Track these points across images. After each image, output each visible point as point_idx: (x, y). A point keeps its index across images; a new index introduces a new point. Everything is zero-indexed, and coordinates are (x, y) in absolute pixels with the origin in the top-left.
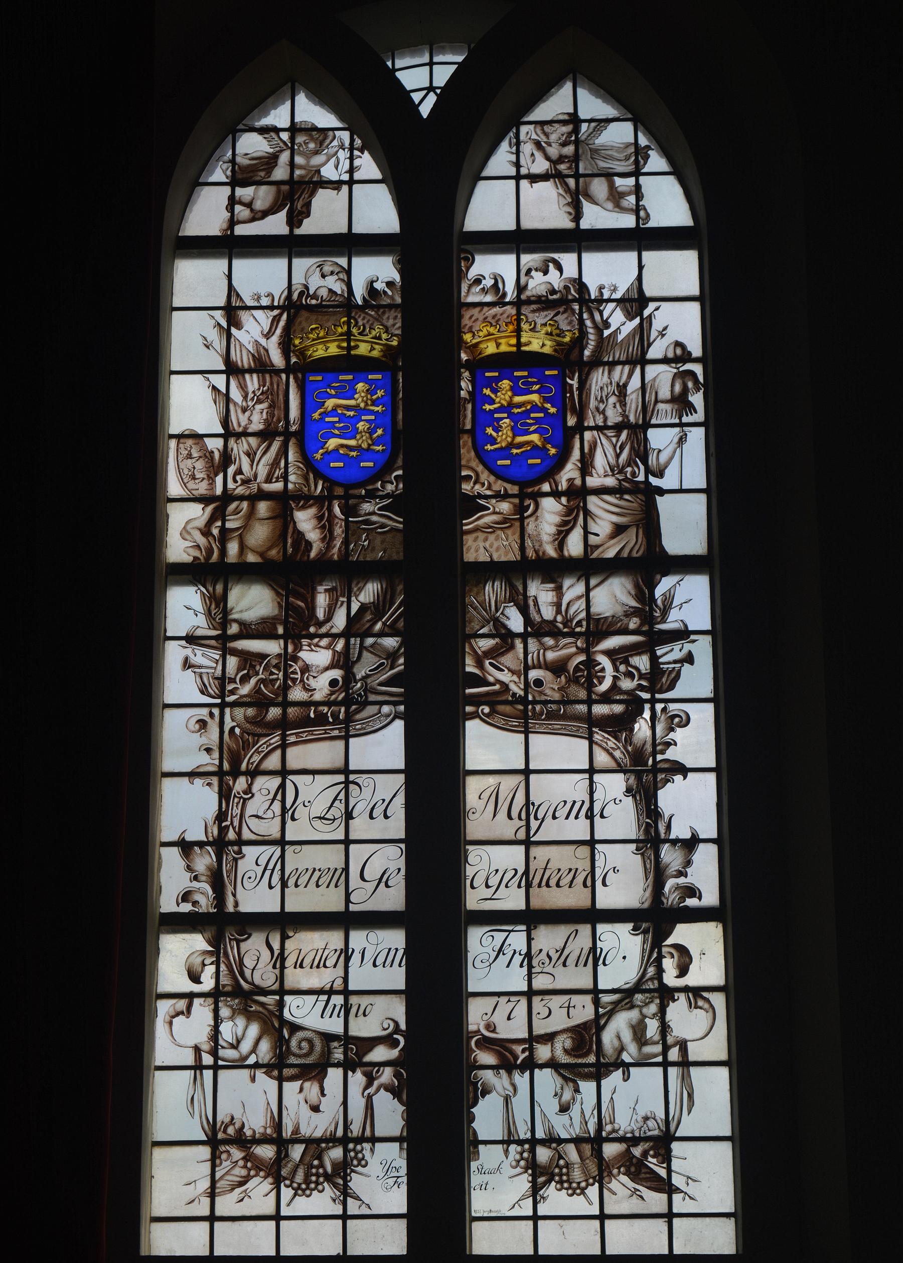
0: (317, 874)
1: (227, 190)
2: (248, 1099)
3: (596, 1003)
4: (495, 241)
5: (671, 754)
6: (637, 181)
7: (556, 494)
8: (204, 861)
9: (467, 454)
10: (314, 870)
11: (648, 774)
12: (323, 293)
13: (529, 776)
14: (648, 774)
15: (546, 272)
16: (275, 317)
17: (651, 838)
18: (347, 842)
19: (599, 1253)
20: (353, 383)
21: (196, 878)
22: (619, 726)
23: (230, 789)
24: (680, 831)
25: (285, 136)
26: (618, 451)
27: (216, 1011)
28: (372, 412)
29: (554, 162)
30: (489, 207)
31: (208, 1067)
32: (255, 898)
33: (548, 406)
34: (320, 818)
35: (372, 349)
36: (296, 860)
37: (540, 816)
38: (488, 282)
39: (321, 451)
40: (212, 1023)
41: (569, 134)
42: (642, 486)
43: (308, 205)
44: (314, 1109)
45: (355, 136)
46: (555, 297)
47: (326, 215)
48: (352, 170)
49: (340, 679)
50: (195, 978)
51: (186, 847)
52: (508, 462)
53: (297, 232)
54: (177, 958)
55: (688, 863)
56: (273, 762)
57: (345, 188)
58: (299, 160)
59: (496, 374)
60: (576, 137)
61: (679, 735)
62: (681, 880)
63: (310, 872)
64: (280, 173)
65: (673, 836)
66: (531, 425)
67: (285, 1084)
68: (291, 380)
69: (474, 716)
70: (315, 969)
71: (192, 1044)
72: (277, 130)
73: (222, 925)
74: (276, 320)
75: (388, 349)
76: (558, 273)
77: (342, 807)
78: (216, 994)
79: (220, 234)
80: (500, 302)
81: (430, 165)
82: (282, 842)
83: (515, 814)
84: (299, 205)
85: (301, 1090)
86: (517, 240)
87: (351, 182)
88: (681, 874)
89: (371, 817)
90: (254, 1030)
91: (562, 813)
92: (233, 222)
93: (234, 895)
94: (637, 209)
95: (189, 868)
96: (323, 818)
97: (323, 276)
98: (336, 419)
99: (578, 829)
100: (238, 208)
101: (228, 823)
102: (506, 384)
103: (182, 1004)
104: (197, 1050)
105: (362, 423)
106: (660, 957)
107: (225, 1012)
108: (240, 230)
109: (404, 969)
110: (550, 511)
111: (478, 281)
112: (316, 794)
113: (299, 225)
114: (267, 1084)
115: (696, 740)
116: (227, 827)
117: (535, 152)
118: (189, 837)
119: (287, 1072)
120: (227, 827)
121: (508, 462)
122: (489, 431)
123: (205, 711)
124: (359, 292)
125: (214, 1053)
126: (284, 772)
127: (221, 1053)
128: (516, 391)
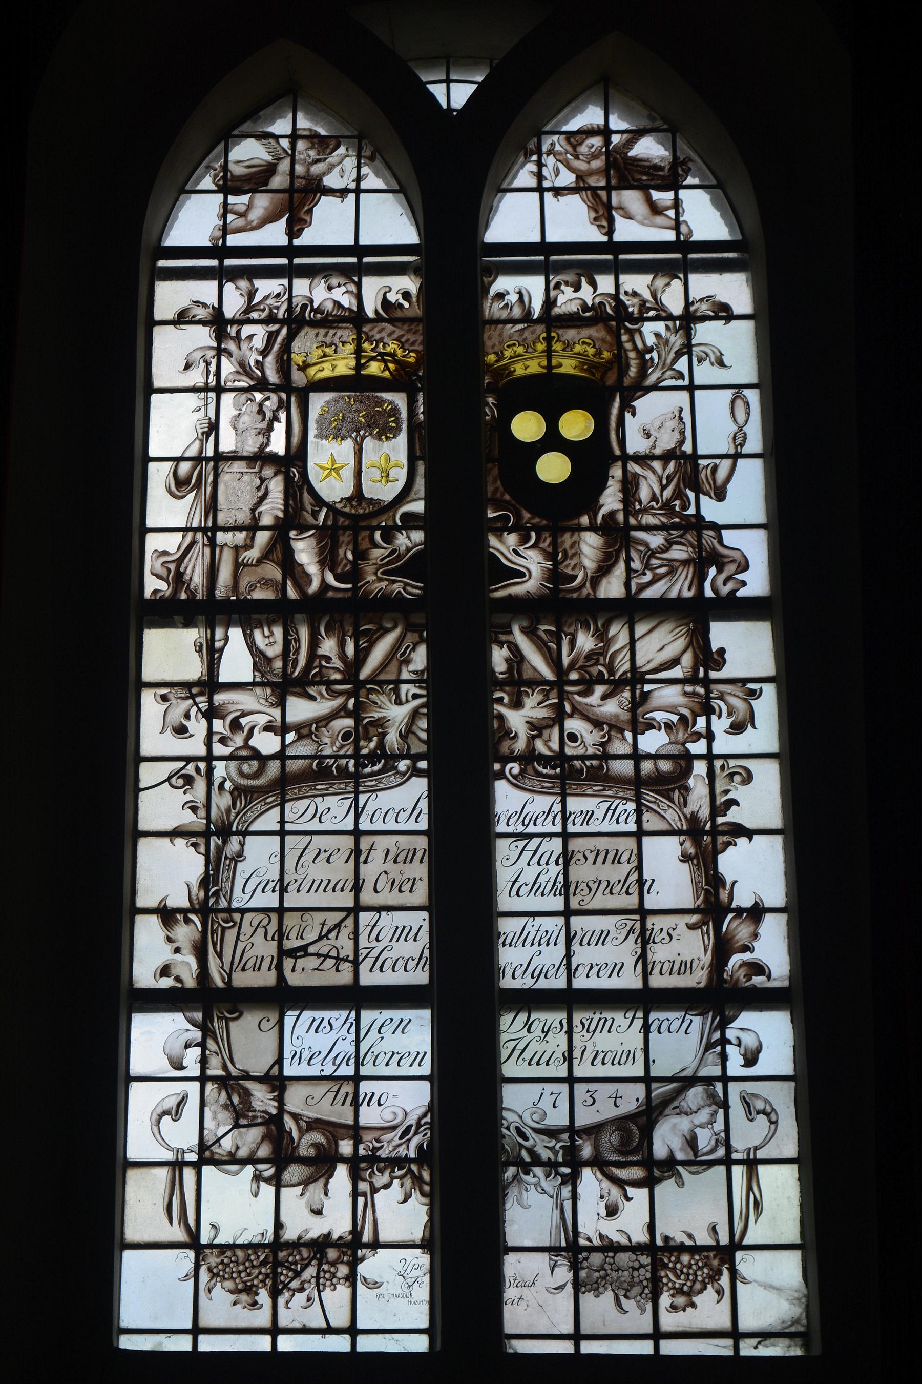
5: (733, 815)
6: (676, 195)
7: (593, 528)
8: (185, 933)
11: (706, 841)
12: (329, 306)
14: (706, 841)
15: (577, 288)
17: (713, 905)
19: (652, 1353)
21: (177, 950)
22: (672, 783)
24: (743, 899)
25: (285, 143)
26: (664, 482)
30: (512, 220)
42: (693, 520)
45: (684, 183)
46: (588, 314)
47: (329, 224)
48: (359, 179)
51: (167, 915)
53: (296, 242)
54: (154, 1040)
57: (352, 197)
58: (299, 169)
62: (747, 956)
64: (278, 181)
68: (293, 399)
70: (338, 892)
72: (277, 137)
73: (209, 1002)
74: (271, 337)
76: (591, 289)
79: (210, 244)
81: (450, 180)
86: (542, 256)
87: (358, 191)
88: (746, 949)
92: (225, 230)
94: (677, 226)
97: (330, 288)
100: (230, 217)
108: (233, 240)
110: (590, 545)
115: (761, 799)
118: (171, 903)
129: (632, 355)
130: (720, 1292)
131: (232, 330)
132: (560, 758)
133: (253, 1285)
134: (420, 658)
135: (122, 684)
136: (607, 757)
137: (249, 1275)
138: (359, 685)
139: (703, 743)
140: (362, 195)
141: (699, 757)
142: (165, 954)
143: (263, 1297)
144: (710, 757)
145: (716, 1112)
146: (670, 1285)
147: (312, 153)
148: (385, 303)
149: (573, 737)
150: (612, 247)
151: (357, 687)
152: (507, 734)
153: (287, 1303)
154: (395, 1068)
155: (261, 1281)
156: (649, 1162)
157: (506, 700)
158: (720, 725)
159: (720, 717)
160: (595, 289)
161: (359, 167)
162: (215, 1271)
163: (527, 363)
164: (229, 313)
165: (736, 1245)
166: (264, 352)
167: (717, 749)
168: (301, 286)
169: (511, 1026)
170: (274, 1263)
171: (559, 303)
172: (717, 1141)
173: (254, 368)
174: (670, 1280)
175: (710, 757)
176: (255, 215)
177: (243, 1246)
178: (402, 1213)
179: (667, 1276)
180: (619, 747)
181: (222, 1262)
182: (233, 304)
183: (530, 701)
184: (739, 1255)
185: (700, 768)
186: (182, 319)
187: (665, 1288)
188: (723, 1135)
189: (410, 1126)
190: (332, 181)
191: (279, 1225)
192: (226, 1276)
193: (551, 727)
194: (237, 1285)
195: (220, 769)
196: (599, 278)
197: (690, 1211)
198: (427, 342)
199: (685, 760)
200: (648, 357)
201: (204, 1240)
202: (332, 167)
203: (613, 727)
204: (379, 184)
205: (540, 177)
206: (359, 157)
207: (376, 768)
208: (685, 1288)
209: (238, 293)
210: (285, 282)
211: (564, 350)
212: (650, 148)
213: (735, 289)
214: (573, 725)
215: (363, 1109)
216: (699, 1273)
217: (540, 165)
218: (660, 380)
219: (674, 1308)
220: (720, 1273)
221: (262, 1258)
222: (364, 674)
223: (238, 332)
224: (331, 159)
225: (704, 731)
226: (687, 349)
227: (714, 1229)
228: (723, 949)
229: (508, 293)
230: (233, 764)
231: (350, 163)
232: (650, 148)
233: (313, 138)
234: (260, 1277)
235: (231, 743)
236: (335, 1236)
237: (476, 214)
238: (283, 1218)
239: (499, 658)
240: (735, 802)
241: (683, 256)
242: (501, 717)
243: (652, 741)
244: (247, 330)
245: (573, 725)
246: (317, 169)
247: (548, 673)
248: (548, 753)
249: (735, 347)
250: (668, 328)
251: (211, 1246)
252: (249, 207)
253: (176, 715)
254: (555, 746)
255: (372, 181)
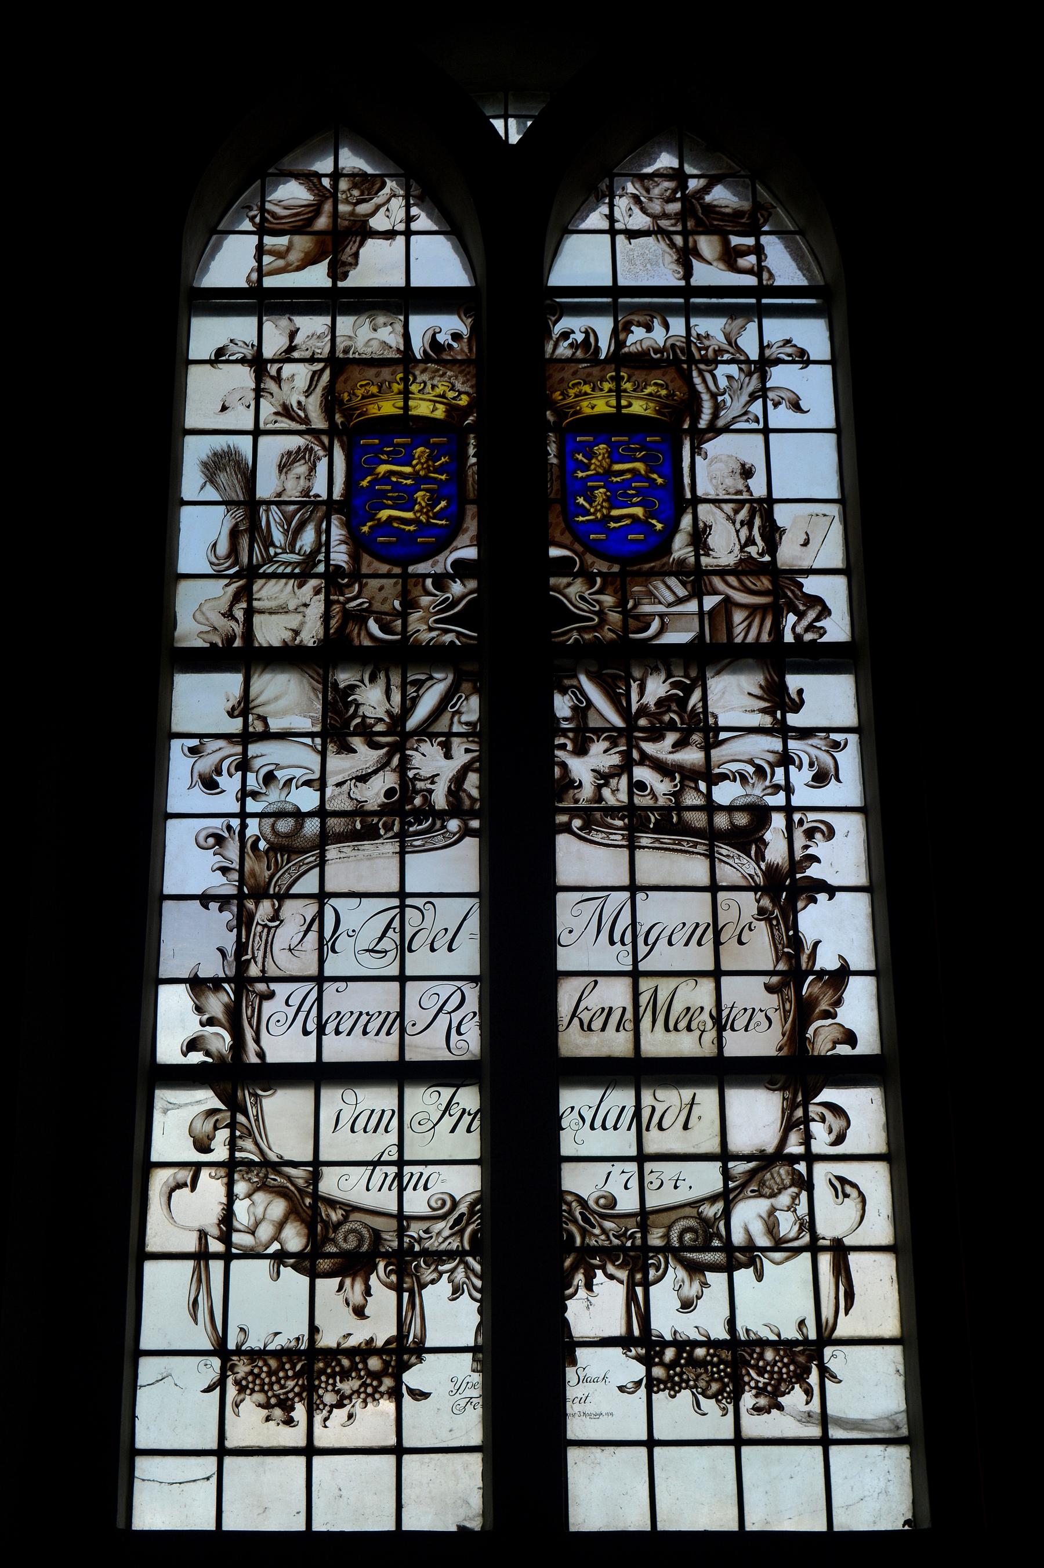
0: (364, 1018)
1: (254, 239)
2: (271, 1306)
3: (726, 1174)
4: (585, 299)
5: (814, 871)
6: (758, 241)
8: (216, 1004)
9: (555, 517)
10: (361, 1014)
11: (788, 890)
13: (630, 923)
15: (649, 329)
16: (314, 373)
18: (402, 979)
20: (410, 448)
21: (211, 1022)
22: (748, 837)
23: (251, 916)
24: (827, 961)
25: (326, 182)
27: (230, 1186)
28: (434, 481)
29: (655, 217)
30: (581, 260)
31: (216, 1256)
32: (284, 1044)
33: (655, 476)
34: (367, 951)
35: (434, 410)
36: (335, 999)
37: (651, 941)
38: (580, 337)
39: (369, 524)
40: (224, 1200)
41: (674, 191)
43: (356, 255)
44: (356, 1316)
47: (377, 265)
48: (409, 219)
49: (397, 787)
50: (203, 1145)
52: (603, 536)
54: (176, 1121)
55: (839, 1002)
56: (309, 884)
57: (401, 240)
58: (343, 208)
59: (591, 439)
60: (683, 193)
61: (820, 848)
63: (355, 1016)
65: (817, 968)
66: (633, 496)
67: (319, 1282)
69: (567, 829)
71: (197, 1225)
73: (236, 1078)
74: (316, 376)
75: (452, 409)
77: (397, 937)
78: (231, 1167)
80: (594, 359)
82: (320, 979)
83: (617, 938)
84: (346, 257)
85: (341, 1288)
86: (613, 298)
87: (408, 233)
89: (433, 950)
90: (278, 1208)
91: (679, 938)
93: (257, 1041)
95: (199, 1009)
96: (372, 951)
98: (389, 487)
99: (701, 958)
100: (267, 259)
101: (248, 957)
102: (601, 448)
103: (186, 1175)
104: (203, 1235)
105: (420, 494)
106: (807, 1120)
107: (241, 1188)
108: (269, 282)
109: (476, 1135)
111: (565, 335)
112: (361, 921)
113: (345, 276)
114: (294, 1281)
115: (843, 855)
116: (248, 961)
117: (633, 207)
119: (324, 1264)
120: (248, 961)
121: (603, 536)
122: (581, 500)
123: (218, 823)
124: (418, 346)
125: (225, 1238)
126: (322, 897)
127: (236, 1238)
128: (615, 457)
129: (705, 397)
130: (808, 1392)
131: (273, 369)
132: (630, 810)
133: (287, 1399)
134: (471, 709)
135: (148, 735)
136: (680, 808)
137: (282, 1387)
138: (406, 736)
139: (782, 794)
140: (413, 238)
141: (778, 809)
142: (192, 1026)
143: (300, 1412)
144: (788, 810)
145: (798, 1195)
146: (752, 1384)
147: (356, 193)
148: (434, 343)
149: (641, 786)
150: (688, 291)
151: (398, 739)
152: (570, 784)
153: (326, 1419)
154: (445, 1150)
155: (296, 1395)
156: (728, 1247)
157: (570, 747)
158: (800, 777)
159: (800, 768)
160: (667, 330)
161: (408, 207)
162: (244, 1383)
163: (594, 402)
164: (268, 353)
165: (826, 1337)
166: (308, 393)
167: (795, 801)
168: (345, 324)
169: (575, 1100)
170: (303, 1375)
171: (628, 344)
172: (801, 1225)
173: (295, 409)
174: (753, 1379)
175: (788, 810)
176: (294, 257)
177: (274, 1354)
178: (452, 1315)
179: (749, 1374)
180: (691, 799)
181: (251, 1373)
182: (274, 344)
183: (598, 747)
184: (828, 1351)
185: (778, 820)
186: (219, 357)
187: (747, 1388)
188: (807, 1218)
189: (462, 1215)
190: (379, 222)
191: (313, 1330)
192: (257, 1388)
193: (619, 775)
194: (269, 1398)
195: (253, 827)
196: (671, 321)
197: (775, 1301)
198: (477, 387)
199: (760, 814)
200: (720, 399)
201: (231, 1345)
202: (378, 208)
203: (688, 776)
204: (431, 226)
205: (611, 218)
206: (407, 197)
207: (425, 825)
208: (769, 1388)
209: (277, 332)
210: (328, 320)
211: (634, 390)
212: (721, 196)
213: (813, 335)
214: (641, 773)
215: (408, 1194)
216: (784, 1370)
217: (611, 206)
218: (735, 420)
219: (758, 1410)
220: (809, 1372)
221: (298, 1368)
222: (412, 723)
223: (279, 370)
224: (377, 201)
225: (782, 783)
226: (762, 393)
227: (802, 1323)
228: (803, 1013)
229: (573, 332)
230: (268, 822)
231: (397, 205)
232: (721, 196)
233: (360, 179)
234: (297, 1390)
235: (264, 798)
236: (380, 1343)
237: (542, 253)
238: (317, 1323)
239: (562, 706)
240: (815, 859)
241: (761, 301)
242: (564, 765)
243: (725, 793)
244: (288, 369)
245: (641, 773)
246: (363, 209)
247: (618, 722)
248: (618, 804)
249: (816, 389)
250: (740, 369)
251: (239, 1352)
252: (289, 249)
253: (205, 764)
254: (623, 797)
255: (423, 222)
